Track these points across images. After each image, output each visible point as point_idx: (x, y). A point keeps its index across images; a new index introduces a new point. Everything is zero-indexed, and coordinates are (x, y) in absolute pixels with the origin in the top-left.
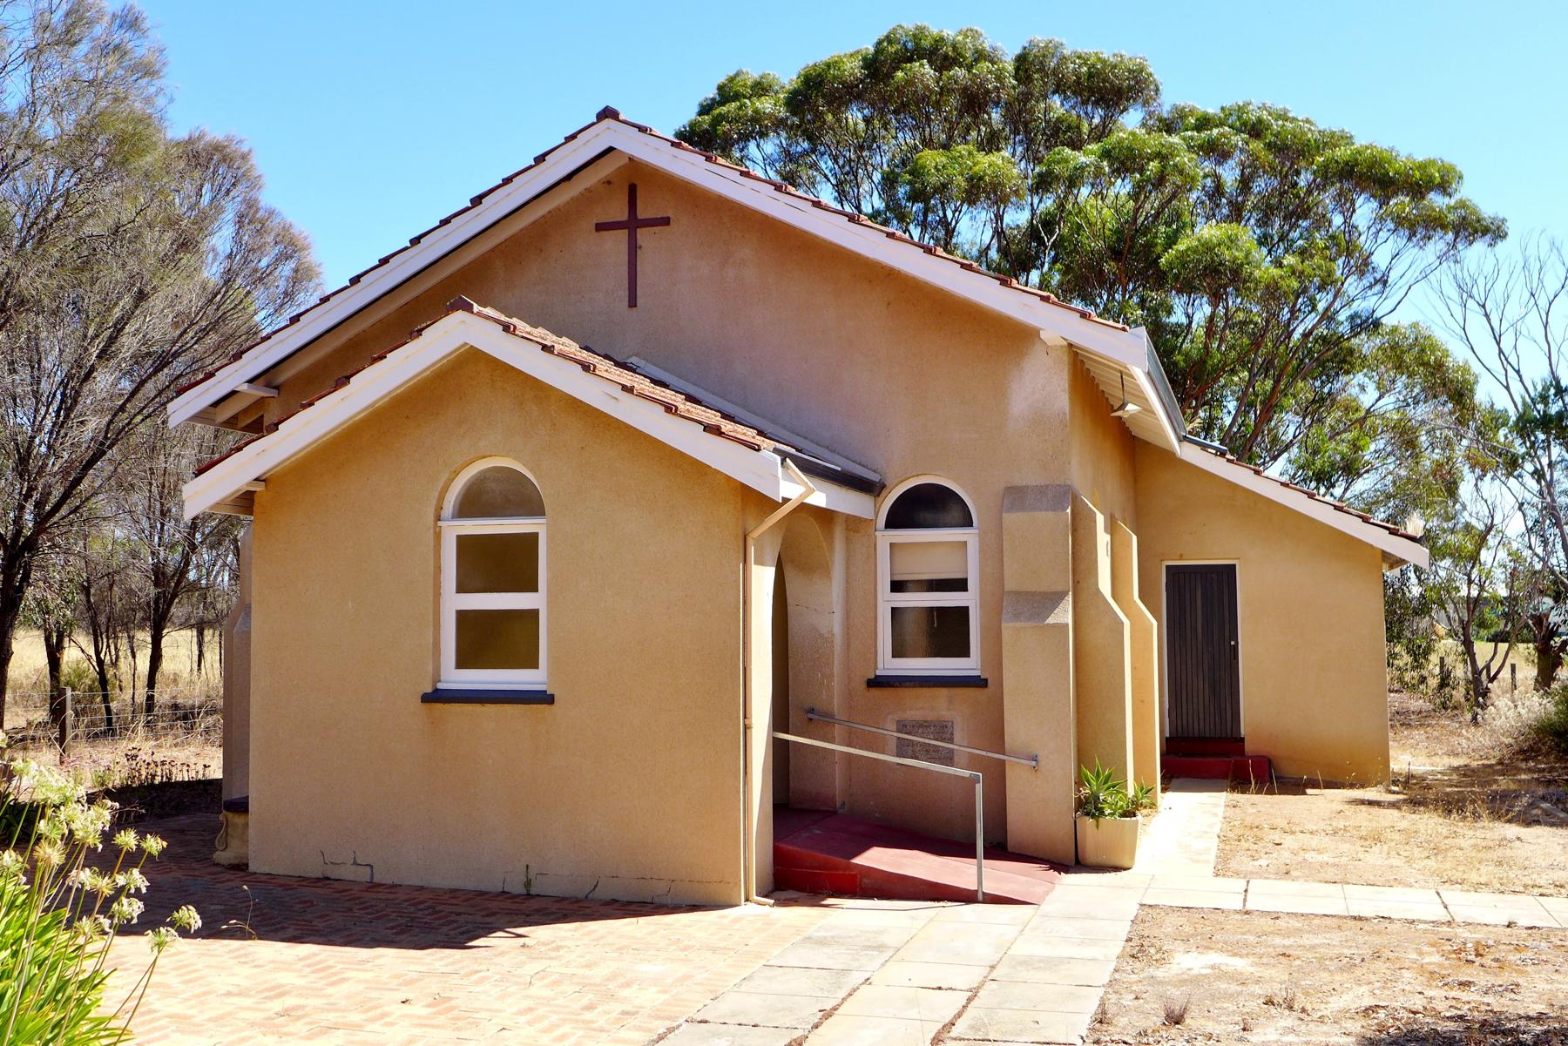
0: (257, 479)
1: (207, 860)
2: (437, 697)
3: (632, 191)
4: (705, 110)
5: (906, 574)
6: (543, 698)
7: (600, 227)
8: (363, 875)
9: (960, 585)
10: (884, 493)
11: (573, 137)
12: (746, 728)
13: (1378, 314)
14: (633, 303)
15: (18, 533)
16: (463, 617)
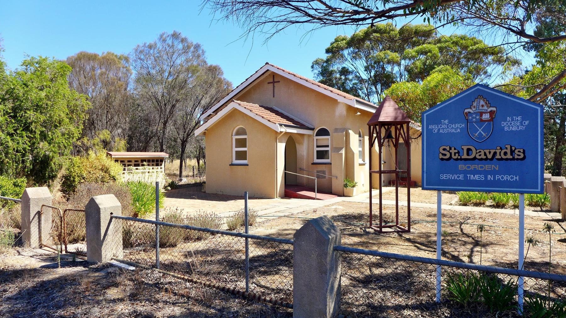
0: (205, 130)
1: (201, 191)
2: (232, 165)
3: (274, 76)
4: (332, 44)
5: (319, 144)
6: (247, 165)
7: (269, 83)
8: (221, 193)
9: (327, 146)
10: (315, 130)
11: (262, 68)
12: (277, 170)
13: (488, 84)
14: (274, 97)
15: (184, 139)
16: (237, 152)
